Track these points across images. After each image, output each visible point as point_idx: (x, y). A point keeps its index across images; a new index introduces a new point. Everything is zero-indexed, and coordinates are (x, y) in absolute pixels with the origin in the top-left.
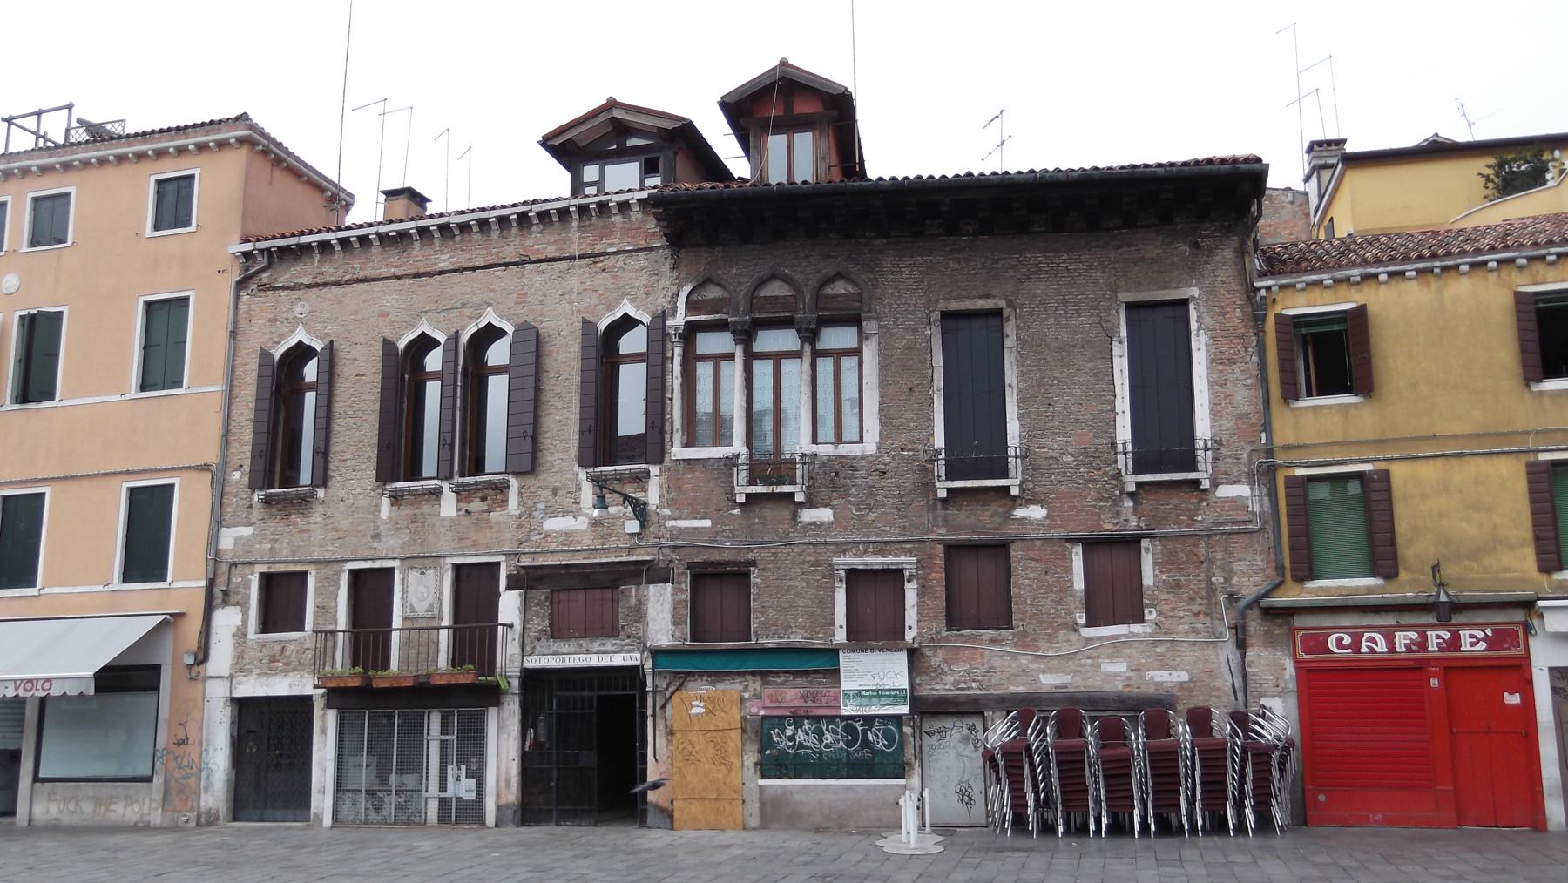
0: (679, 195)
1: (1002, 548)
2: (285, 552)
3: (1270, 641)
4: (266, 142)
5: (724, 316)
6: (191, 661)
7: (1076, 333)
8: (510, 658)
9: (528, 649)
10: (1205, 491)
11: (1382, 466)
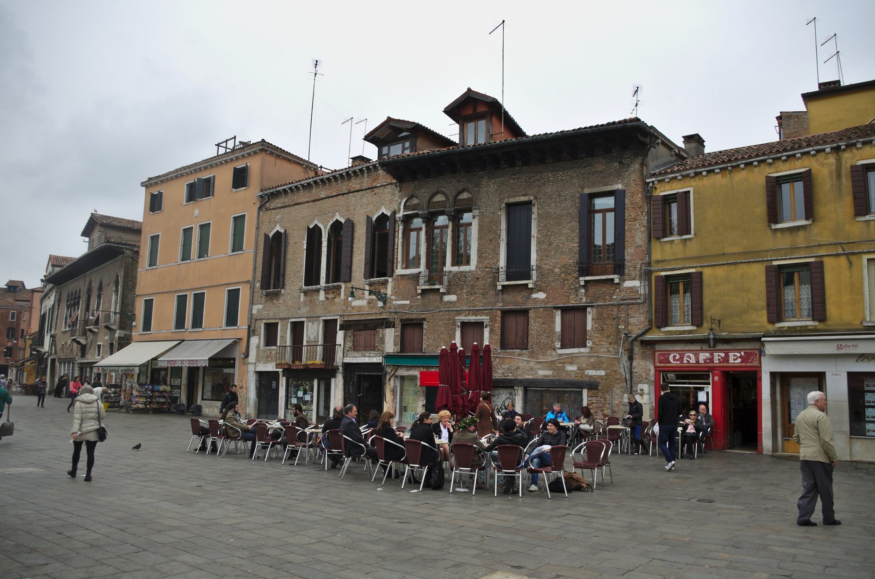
0: (410, 158)
1: (525, 312)
2: (272, 315)
3: (644, 357)
4: (271, 150)
5: (418, 211)
6: (243, 357)
7: (564, 210)
8: (340, 358)
9: (345, 355)
10: (617, 284)
11: (699, 270)
